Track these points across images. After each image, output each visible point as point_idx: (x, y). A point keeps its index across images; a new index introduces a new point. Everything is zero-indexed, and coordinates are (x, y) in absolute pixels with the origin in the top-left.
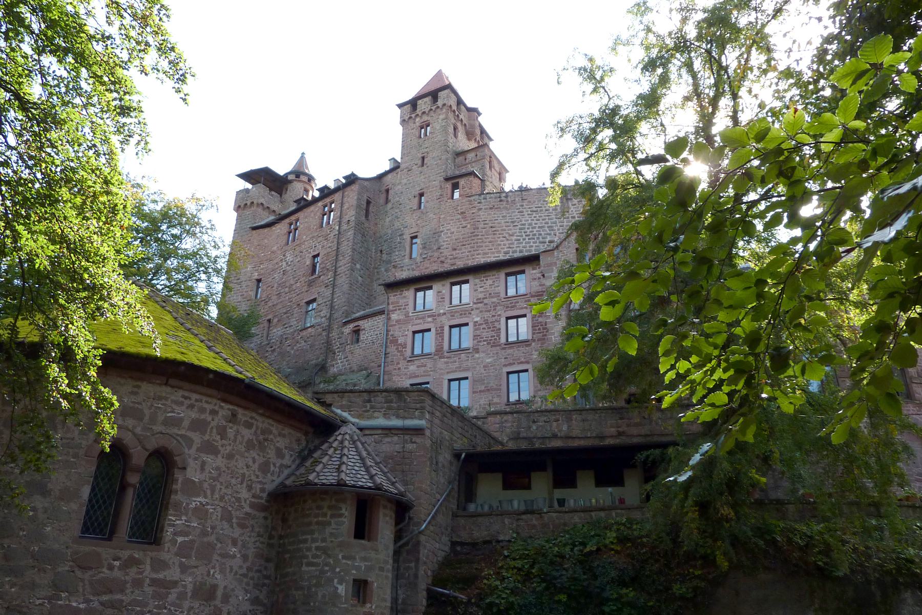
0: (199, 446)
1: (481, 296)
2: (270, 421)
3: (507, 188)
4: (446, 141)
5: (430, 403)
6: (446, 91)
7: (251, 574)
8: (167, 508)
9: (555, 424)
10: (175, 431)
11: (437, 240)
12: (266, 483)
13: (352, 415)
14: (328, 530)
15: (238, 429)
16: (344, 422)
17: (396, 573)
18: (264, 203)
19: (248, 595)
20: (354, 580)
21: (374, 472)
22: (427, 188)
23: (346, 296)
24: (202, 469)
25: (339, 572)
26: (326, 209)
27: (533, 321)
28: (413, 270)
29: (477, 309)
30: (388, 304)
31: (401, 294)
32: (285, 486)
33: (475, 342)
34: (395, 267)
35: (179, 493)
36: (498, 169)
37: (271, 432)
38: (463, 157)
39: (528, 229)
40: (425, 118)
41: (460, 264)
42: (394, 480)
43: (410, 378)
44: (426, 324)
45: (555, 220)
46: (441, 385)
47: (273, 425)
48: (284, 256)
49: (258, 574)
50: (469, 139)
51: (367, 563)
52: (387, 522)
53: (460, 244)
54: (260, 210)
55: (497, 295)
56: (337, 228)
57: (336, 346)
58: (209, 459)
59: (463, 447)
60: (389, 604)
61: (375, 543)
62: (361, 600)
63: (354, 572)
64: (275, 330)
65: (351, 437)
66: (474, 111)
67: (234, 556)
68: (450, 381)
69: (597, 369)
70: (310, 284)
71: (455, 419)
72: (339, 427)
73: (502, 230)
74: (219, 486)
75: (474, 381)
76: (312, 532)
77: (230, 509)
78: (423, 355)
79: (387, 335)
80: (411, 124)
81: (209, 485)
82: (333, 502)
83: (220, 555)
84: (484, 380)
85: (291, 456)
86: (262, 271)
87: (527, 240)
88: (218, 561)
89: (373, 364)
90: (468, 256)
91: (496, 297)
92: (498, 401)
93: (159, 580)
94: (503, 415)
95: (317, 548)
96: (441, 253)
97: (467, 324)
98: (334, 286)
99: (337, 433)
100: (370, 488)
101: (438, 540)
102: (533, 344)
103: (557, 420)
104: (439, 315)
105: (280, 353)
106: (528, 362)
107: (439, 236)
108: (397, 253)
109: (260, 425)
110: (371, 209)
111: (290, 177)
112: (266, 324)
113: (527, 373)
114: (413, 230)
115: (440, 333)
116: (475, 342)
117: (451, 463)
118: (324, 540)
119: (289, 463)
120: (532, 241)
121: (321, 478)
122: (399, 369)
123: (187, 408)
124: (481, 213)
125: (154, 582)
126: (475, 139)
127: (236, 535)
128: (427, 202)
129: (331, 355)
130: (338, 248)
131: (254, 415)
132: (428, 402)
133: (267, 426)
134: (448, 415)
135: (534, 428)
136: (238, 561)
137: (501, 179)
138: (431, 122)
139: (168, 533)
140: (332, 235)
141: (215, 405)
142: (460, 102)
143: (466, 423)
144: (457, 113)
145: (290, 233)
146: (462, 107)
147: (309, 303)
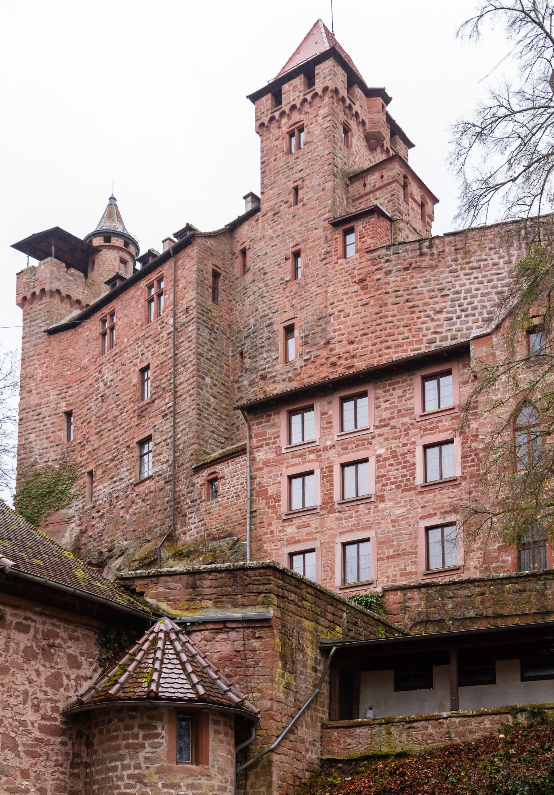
1: (386, 415)
2: (55, 621)
3: (434, 233)
9: (479, 598)
11: (324, 330)
13: (171, 606)
14: (142, 754)
15: (8, 635)
16: (158, 615)
18: (62, 290)
23: (194, 428)
26: (153, 291)
27: (463, 448)
28: (291, 380)
29: (380, 435)
31: (268, 421)
33: (379, 485)
34: (263, 378)
37: (57, 636)
39: (465, 299)
40: (296, 117)
43: (287, 545)
44: (308, 465)
47: (59, 627)
48: (100, 372)
50: (372, 149)
51: (195, 792)
54: (56, 299)
56: (171, 321)
61: (206, 766)
64: (100, 487)
68: (344, 545)
70: (142, 413)
72: (154, 623)
75: (379, 543)
76: (122, 758)
77: (13, 735)
79: (252, 484)
82: (145, 720)
84: (393, 541)
85: (91, 664)
86: (72, 400)
87: (463, 318)
92: (414, 570)
95: (130, 777)
97: (366, 460)
98: (175, 414)
100: (191, 700)
102: (463, 484)
104: (325, 449)
108: (265, 355)
109: (40, 627)
111: (97, 242)
112: (86, 479)
114: (286, 316)
115: (327, 476)
116: (379, 485)
118: (137, 766)
119: (89, 674)
120: (471, 319)
122: (272, 532)
124: (391, 278)
127: (26, 766)
128: (306, 266)
129: (180, 519)
130: (176, 354)
131: (29, 614)
133: (50, 628)
138: (306, 122)
140: (165, 334)
144: (348, 102)
145: (104, 334)
146: (358, 91)
147: (142, 443)
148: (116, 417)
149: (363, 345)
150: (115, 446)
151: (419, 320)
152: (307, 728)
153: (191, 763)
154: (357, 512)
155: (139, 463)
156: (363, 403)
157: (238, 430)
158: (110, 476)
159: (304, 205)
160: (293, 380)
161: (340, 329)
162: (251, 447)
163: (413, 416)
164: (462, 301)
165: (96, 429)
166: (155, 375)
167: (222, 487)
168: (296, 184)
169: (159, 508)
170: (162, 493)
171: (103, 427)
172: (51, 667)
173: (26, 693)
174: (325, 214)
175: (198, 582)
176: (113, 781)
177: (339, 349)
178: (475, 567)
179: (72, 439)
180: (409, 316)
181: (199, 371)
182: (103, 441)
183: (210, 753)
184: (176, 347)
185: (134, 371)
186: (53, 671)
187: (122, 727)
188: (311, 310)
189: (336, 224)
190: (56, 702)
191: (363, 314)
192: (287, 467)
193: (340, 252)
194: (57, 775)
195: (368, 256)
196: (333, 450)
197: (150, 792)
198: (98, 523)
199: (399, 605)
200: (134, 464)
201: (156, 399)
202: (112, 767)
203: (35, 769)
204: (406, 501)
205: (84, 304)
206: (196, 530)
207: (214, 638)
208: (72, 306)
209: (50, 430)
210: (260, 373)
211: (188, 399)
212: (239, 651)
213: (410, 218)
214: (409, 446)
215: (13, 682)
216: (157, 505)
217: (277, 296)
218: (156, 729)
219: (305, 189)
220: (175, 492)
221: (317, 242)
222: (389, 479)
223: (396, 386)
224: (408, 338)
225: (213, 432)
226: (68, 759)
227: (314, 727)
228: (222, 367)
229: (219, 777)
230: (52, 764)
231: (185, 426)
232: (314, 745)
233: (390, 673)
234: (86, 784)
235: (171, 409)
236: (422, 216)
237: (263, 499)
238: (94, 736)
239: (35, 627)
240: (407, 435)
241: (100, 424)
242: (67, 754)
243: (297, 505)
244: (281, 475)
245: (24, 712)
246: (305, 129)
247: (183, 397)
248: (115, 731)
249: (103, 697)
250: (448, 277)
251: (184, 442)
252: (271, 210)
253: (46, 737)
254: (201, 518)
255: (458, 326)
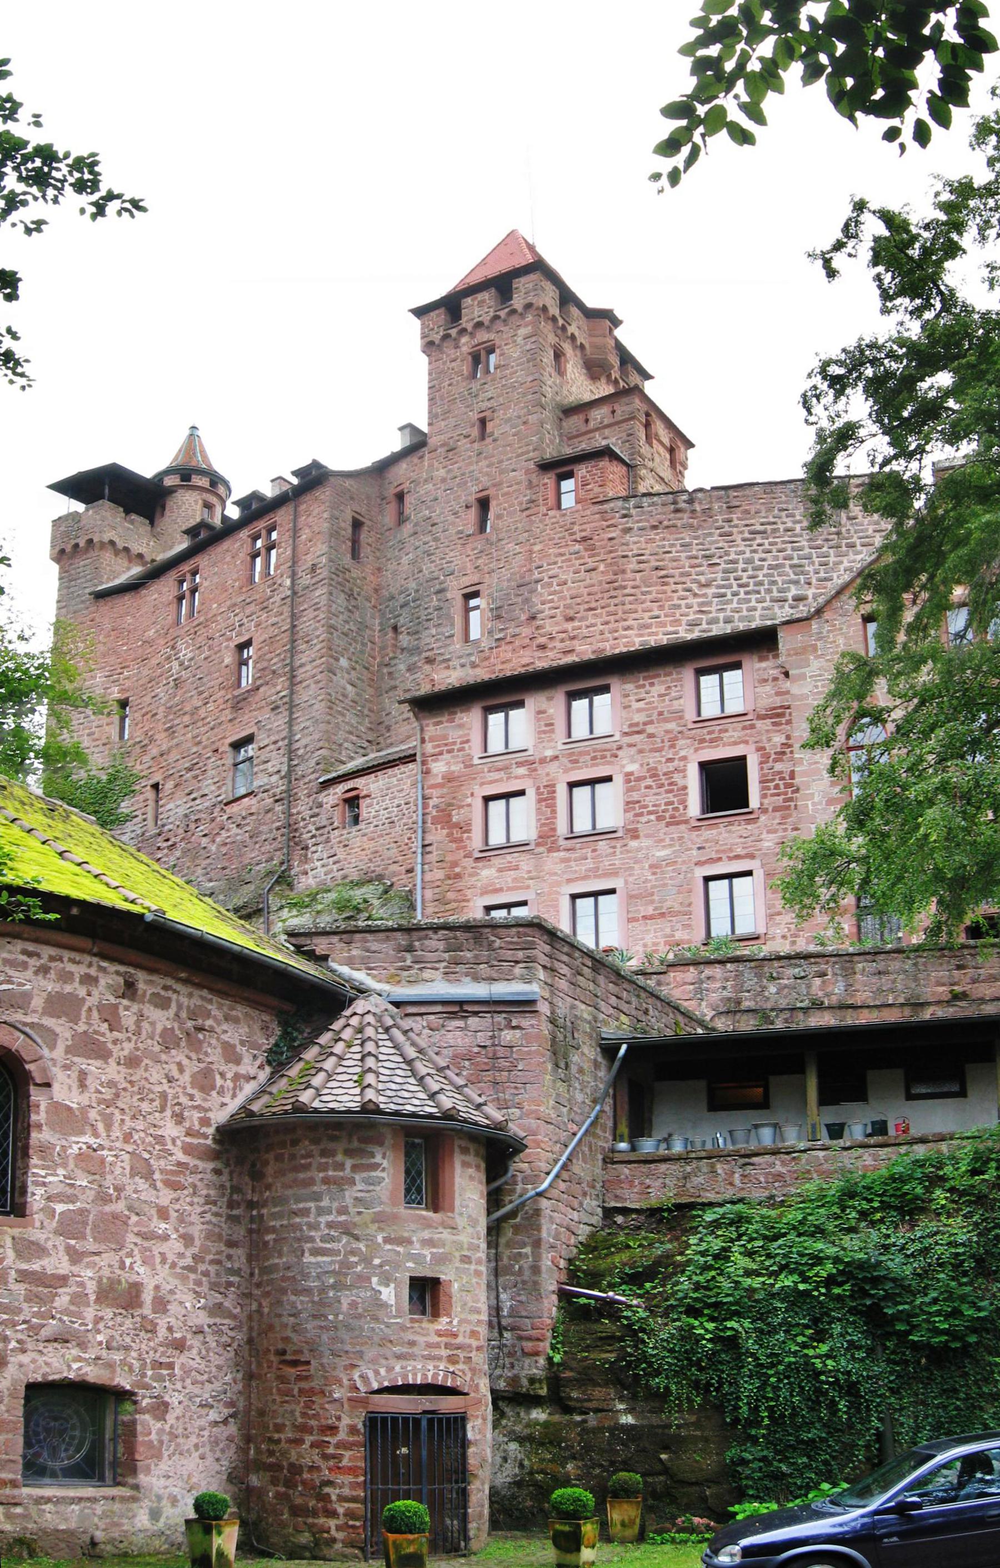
0: (70, 1043)
1: (639, 718)
2: (205, 993)
3: (691, 482)
4: (539, 381)
5: (547, 948)
6: (533, 277)
7: (202, 1267)
8: (26, 1155)
9: (818, 981)
10: (18, 1017)
11: (527, 601)
12: (210, 1110)
13: (374, 977)
14: (350, 1194)
15: (140, 1011)
16: (362, 991)
17: (493, 1264)
19: (203, 1301)
20: (412, 1278)
21: (435, 1087)
22: (497, 485)
23: (323, 727)
24: (82, 1085)
25: (381, 1266)
26: (259, 544)
27: (762, 769)
28: (474, 665)
29: (630, 745)
30: (423, 741)
32: (251, 1114)
33: (630, 815)
34: (430, 661)
35: (44, 1128)
36: (666, 441)
37: (208, 1015)
38: (582, 417)
39: (744, 570)
40: (482, 336)
41: (585, 651)
42: (480, 1100)
43: (482, 894)
45: (807, 551)
46: (556, 908)
47: (210, 1001)
48: (173, 648)
49: (217, 1267)
50: (594, 377)
51: (435, 1250)
52: (471, 1178)
53: (582, 607)
55: (678, 715)
56: (288, 582)
57: (307, 832)
58: (92, 1065)
59: (620, 1034)
60: (484, 1317)
61: (450, 1214)
62: (428, 1309)
63: (410, 1264)
64: (171, 806)
65: (379, 1018)
66: (607, 318)
67: (166, 1238)
68: (574, 897)
69: (988, 516)
71: (601, 979)
72: (352, 1001)
73: (682, 575)
74: (118, 1116)
75: (631, 898)
76: (317, 1197)
77: (146, 1156)
78: (509, 847)
79: (425, 806)
80: (450, 351)
81: (100, 1113)
82: (355, 1144)
83: (138, 1234)
84: (652, 894)
85: (255, 1057)
86: (128, 684)
87: (742, 596)
88: (136, 1244)
89: (394, 868)
90: (602, 633)
91: (675, 719)
93: (34, 1273)
94: (702, 967)
95: (330, 1225)
96: (538, 628)
97: (608, 779)
98: (291, 707)
99: (347, 1013)
100: (430, 1116)
101: (576, 1205)
103: (822, 974)
104: (543, 761)
105: (185, 852)
106: (751, 856)
107: (533, 591)
109: (185, 1001)
110: (364, 536)
111: (169, 482)
112: (150, 794)
113: (749, 878)
114: (466, 581)
115: (546, 799)
117: (596, 1065)
118: (343, 1211)
119: (252, 1071)
120: (753, 597)
121: (325, 1098)
123: (36, 973)
125: (24, 1276)
126: (609, 376)
129: (298, 852)
131: (170, 982)
132: (541, 948)
133: (199, 1002)
134: (586, 971)
135: (773, 989)
136: (174, 1246)
137: (677, 465)
138: (497, 342)
139: (37, 1197)
140: (277, 598)
141: (90, 965)
142: (567, 298)
143: (626, 985)
144: (561, 322)
145: (180, 598)
146: (575, 311)
148: (196, 708)
149: (588, 623)
150: (195, 750)
151: (675, 595)
152: (585, 1161)
153: (427, 1209)
154: (594, 851)
155: (231, 774)
156: (601, 701)
157: (389, 730)
158: (187, 791)
159: (494, 440)
160: (477, 666)
161: (552, 601)
162: (423, 754)
163: (682, 722)
164: (740, 573)
165: (164, 723)
166: (260, 653)
167: (365, 810)
168: (482, 415)
169: (264, 837)
170: (270, 815)
171: (176, 722)
172: (199, 1060)
173: (164, 1096)
174: (528, 452)
175: (417, 943)
176: (301, 1230)
177: (549, 627)
178: (784, 937)
179: (126, 737)
180: (659, 588)
181: (330, 649)
182: (175, 741)
183: (457, 1195)
184: (294, 616)
185: (227, 647)
186: (202, 1065)
187: (316, 1153)
188: (505, 573)
189: (545, 467)
190: (206, 1110)
191: (588, 581)
192: (482, 784)
193: (552, 501)
194: (208, 1216)
195: (597, 508)
196: (556, 763)
197: (364, 1249)
198: (167, 855)
199: (692, 987)
200: (224, 774)
201: (261, 685)
202: (300, 1210)
203: (177, 1207)
204: (672, 839)
205: (148, 559)
206: (325, 869)
207: (443, 1026)
208: (130, 561)
209: (95, 724)
210: (424, 655)
211: (313, 686)
212: (484, 1047)
213: (655, 464)
214: (676, 762)
215: (146, 1079)
216: (261, 832)
217: (452, 554)
218: (373, 1157)
219: (497, 421)
220: (291, 815)
221: (515, 487)
222: (645, 807)
223: (656, 681)
224: (657, 617)
225: (351, 733)
226: (223, 1195)
227: (594, 1159)
228: (364, 644)
229: (470, 1230)
230: (202, 1200)
231: (308, 723)
232: (594, 1187)
233: (702, 1084)
234: (250, 1231)
235: (285, 700)
236: (671, 462)
237: (442, 828)
238: (266, 1163)
239: (178, 1001)
240: (673, 746)
241: (171, 717)
242: (222, 1187)
243: (497, 837)
244: (472, 795)
245: (162, 1123)
246: (498, 351)
247: (304, 684)
248: (303, 1157)
249: (289, 1107)
250: (717, 542)
251: (306, 746)
252: (442, 445)
253: (192, 1162)
254: (332, 852)
255: (735, 605)
